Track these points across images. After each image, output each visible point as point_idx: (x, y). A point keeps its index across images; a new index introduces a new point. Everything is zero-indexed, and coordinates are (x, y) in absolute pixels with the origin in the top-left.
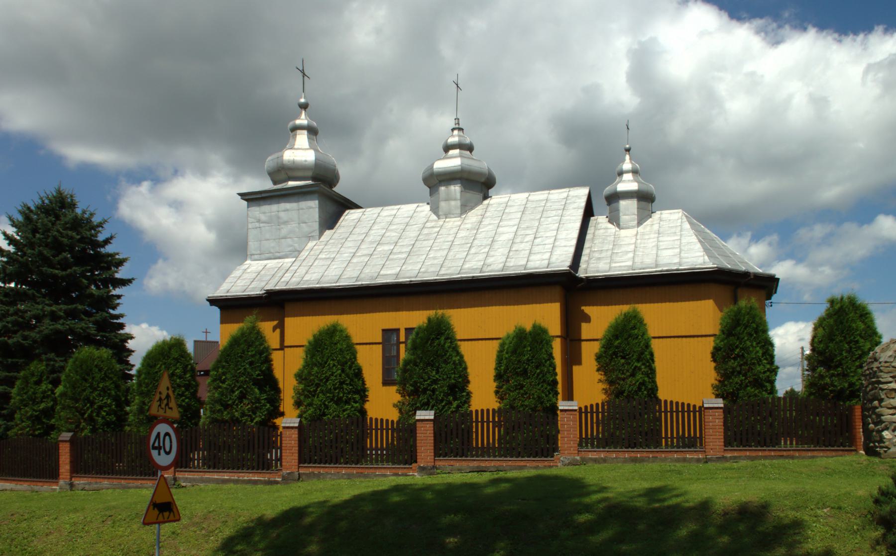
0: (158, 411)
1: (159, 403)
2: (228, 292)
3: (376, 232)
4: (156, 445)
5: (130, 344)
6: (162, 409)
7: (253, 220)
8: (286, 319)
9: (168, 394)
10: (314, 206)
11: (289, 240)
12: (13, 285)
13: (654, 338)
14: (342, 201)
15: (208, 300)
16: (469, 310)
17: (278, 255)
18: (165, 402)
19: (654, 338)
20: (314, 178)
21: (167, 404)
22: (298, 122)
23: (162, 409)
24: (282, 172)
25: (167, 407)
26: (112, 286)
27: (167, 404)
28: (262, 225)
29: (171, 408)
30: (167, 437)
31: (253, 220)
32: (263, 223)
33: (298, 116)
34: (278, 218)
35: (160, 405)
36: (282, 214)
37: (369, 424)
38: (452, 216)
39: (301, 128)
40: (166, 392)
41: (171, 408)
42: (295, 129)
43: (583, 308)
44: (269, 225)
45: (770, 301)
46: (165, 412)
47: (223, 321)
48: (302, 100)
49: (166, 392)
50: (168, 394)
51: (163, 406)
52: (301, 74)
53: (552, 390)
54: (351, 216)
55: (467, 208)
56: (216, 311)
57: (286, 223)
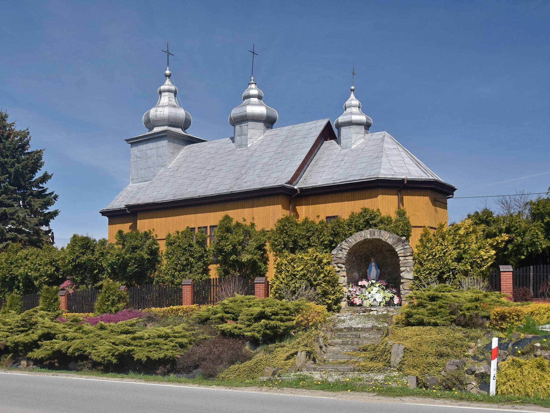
5: (44, 183)
7: (134, 156)
8: (138, 221)
10: (165, 145)
11: (152, 168)
12: (548, 261)
13: (414, 227)
14: (188, 139)
15: (100, 212)
16: (189, 215)
17: (146, 179)
19: (414, 227)
22: (162, 87)
24: (150, 124)
26: (12, 356)
28: (138, 159)
31: (134, 156)
32: (139, 158)
33: (163, 83)
34: (147, 154)
36: (149, 152)
38: (243, 146)
44: (142, 159)
47: (110, 223)
52: (166, 55)
56: (106, 219)
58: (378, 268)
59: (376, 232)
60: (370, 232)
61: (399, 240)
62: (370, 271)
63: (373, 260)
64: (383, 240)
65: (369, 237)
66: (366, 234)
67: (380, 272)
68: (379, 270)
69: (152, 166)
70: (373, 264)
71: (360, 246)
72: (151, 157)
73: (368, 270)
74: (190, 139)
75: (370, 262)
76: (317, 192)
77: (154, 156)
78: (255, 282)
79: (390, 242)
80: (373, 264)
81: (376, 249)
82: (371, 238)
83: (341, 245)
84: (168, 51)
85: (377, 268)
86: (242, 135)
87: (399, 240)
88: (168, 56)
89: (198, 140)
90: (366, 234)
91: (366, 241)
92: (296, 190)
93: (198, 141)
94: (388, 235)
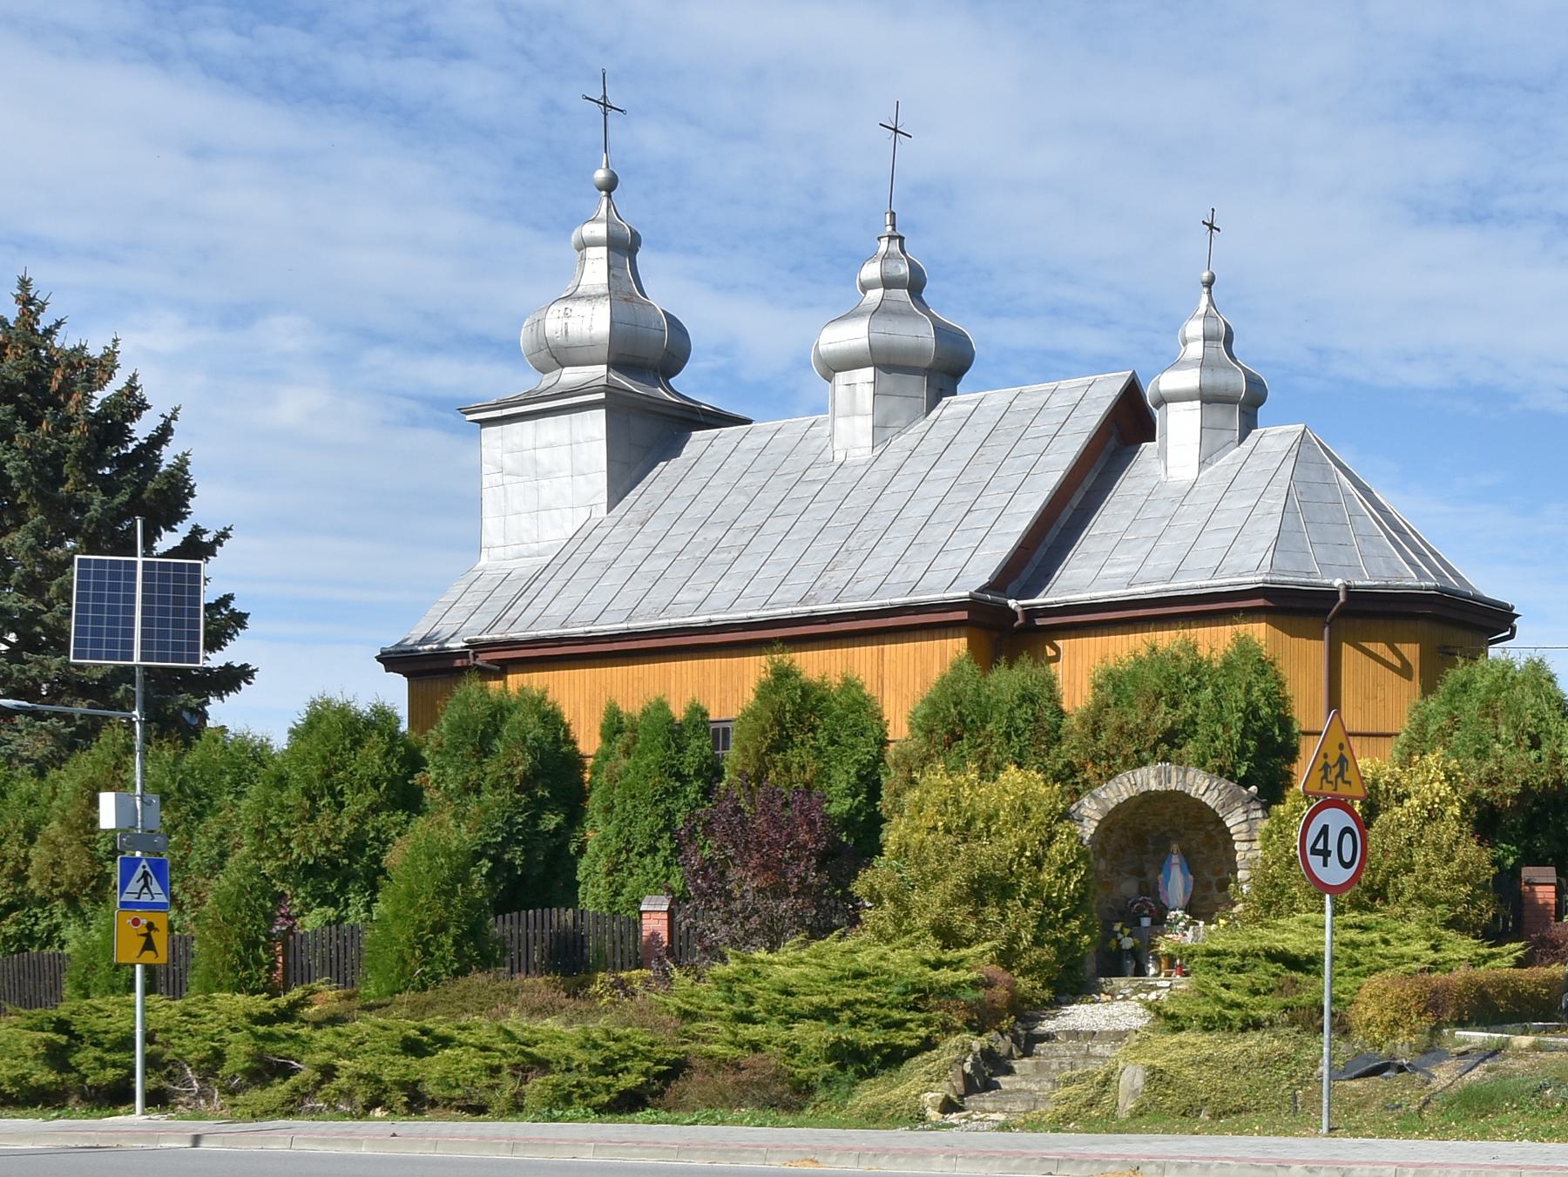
0: (1321, 788)
1: (1322, 773)
2: (563, 626)
3: (736, 464)
4: (1320, 846)
6: (1331, 782)
9: (1342, 755)
17: (535, 547)
18: (1336, 770)
20: (614, 365)
21: (1341, 774)
23: (1331, 782)
25: (1339, 779)
27: (1341, 774)
28: (507, 479)
29: (1349, 783)
30: (1348, 837)
34: (536, 462)
35: (1325, 777)
36: (542, 455)
37: (666, 1068)
39: (595, 243)
40: (1339, 752)
41: (1349, 783)
42: (584, 245)
43: (1344, 644)
44: (520, 479)
45: (183, 530)
46: (1335, 790)
48: (601, 175)
49: (1339, 752)
50: (1342, 755)
51: (1331, 777)
52: (599, 109)
53: (1249, 1025)
54: (699, 439)
55: (889, 432)
57: (548, 474)
58: (1189, 867)
59: (1174, 774)
60: (1159, 772)
61: (1235, 797)
62: (1167, 878)
63: (1175, 847)
64: (1192, 795)
65: (1154, 786)
66: (1148, 779)
67: (1195, 881)
68: (1191, 877)
69: (554, 506)
70: (1175, 859)
71: (1137, 808)
72: (550, 472)
73: (1161, 876)
74: (686, 415)
75: (1169, 853)
76: (1075, 501)
77: (560, 471)
78: (643, 908)
79: (1211, 800)
80: (1175, 859)
81: (1186, 819)
82: (1162, 788)
83: (1079, 807)
84: (605, 97)
85: (1186, 869)
86: (854, 414)
87: (1235, 797)
88: (605, 114)
89: (712, 416)
90: (1148, 779)
91: (1148, 798)
92: (1013, 614)
93: (713, 421)
94: (1207, 782)
